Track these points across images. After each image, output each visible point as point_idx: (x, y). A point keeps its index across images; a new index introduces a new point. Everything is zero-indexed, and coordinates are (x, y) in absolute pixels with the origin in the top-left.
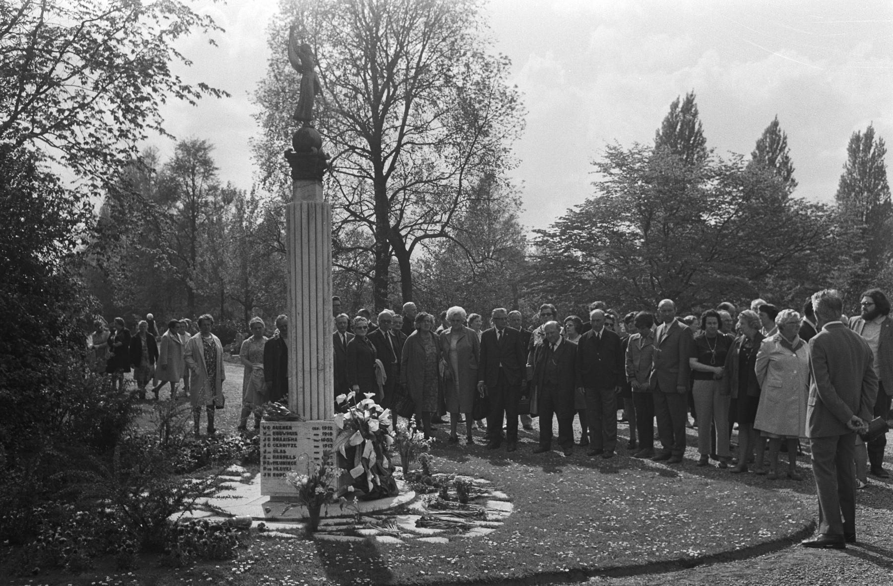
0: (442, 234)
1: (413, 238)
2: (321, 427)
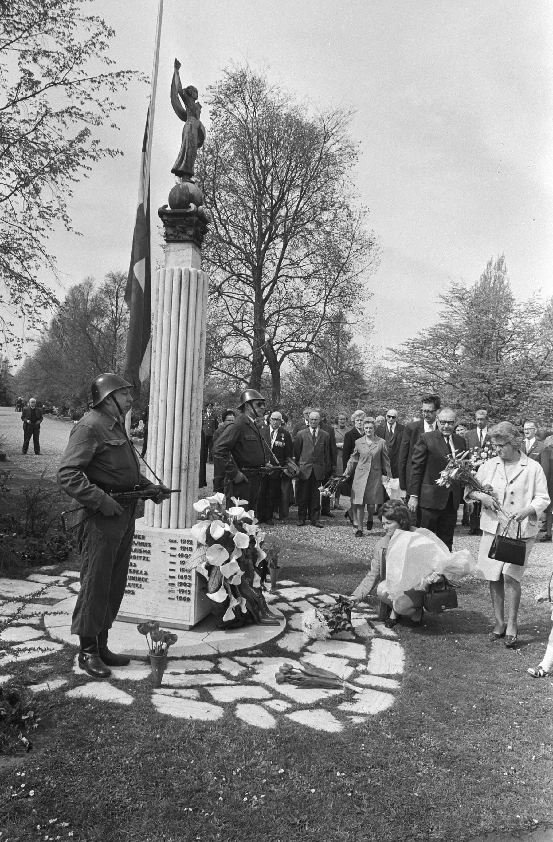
0: (307, 350)
1: (283, 353)
2: (179, 540)
